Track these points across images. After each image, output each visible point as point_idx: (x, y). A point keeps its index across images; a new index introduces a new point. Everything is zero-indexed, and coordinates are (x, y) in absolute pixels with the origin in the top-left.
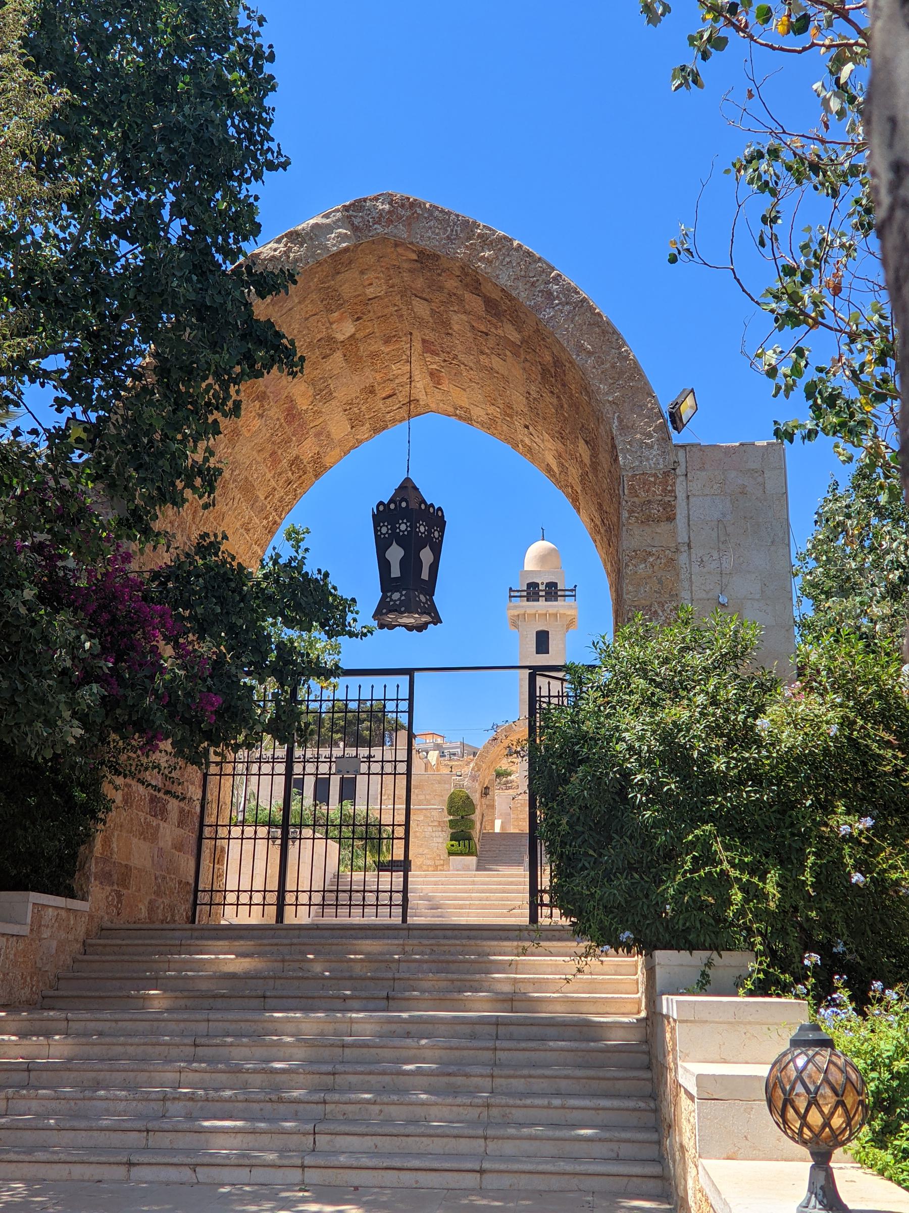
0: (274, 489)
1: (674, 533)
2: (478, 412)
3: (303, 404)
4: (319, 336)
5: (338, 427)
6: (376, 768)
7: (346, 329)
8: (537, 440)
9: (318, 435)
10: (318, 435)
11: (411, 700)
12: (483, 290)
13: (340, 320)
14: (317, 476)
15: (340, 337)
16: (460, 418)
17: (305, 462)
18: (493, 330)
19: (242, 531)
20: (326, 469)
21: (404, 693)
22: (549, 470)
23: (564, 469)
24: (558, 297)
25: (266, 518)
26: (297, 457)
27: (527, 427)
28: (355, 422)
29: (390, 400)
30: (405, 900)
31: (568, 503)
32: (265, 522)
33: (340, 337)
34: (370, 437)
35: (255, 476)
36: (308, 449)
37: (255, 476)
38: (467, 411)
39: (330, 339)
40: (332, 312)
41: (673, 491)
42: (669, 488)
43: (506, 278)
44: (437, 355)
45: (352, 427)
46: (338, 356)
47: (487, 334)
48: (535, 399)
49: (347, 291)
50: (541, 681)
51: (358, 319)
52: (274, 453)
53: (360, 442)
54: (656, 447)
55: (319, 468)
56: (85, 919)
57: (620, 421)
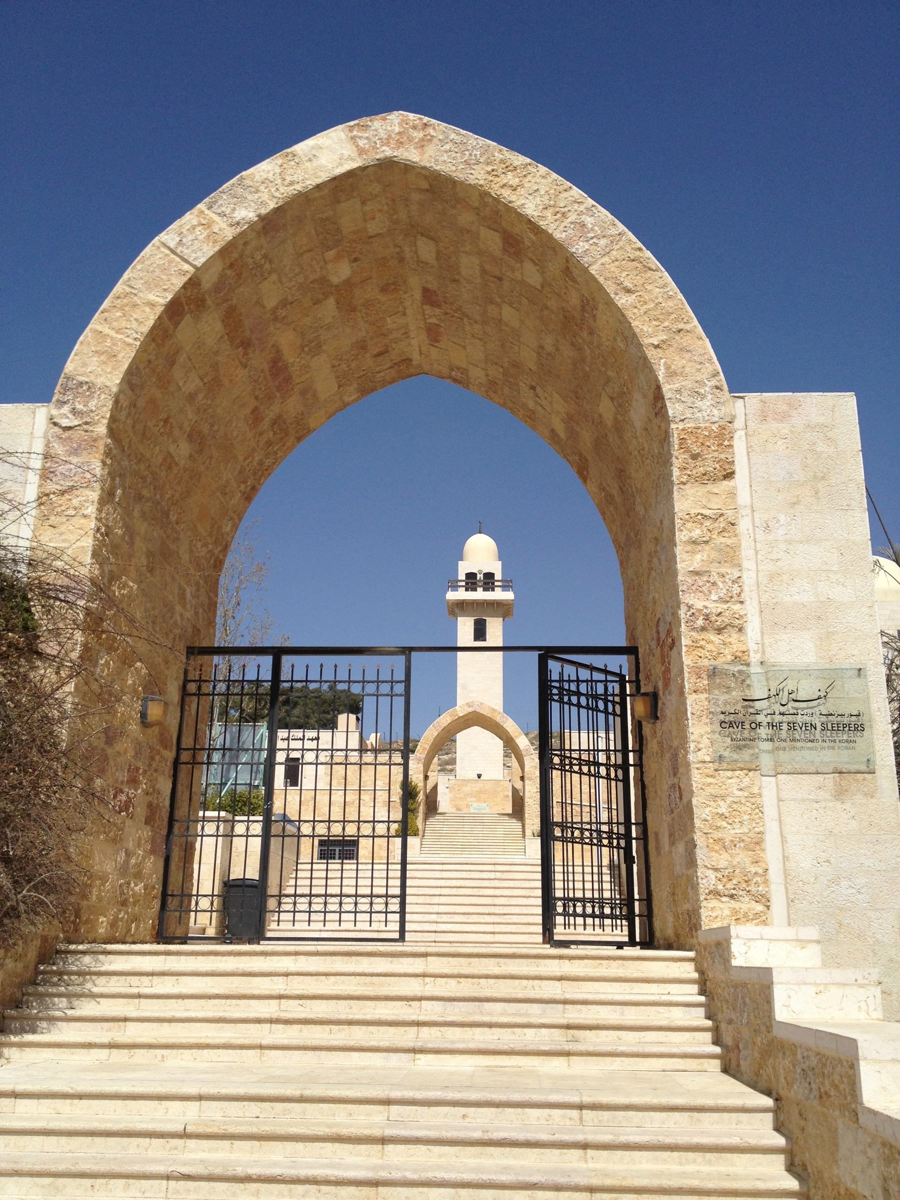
0: (254, 450)
1: (732, 494)
2: (477, 374)
3: (290, 357)
4: (312, 277)
5: (325, 384)
6: (324, 757)
7: (342, 272)
8: (544, 402)
9: (304, 392)
10: (304, 392)
11: (407, 681)
12: (504, 224)
13: (338, 257)
14: (299, 439)
15: (335, 280)
16: (455, 380)
17: (288, 421)
18: (509, 274)
19: (218, 494)
20: (309, 431)
21: (400, 675)
22: (553, 435)
23: (573, 434)
24: (592, 229)
25: (245, 482)
26: (280, 416)
27: (533, 388)
28: (342, 381)
29: (381, 358)
30: (403, 904)
31: (571, 474)
32: (243, 486)
33: (335, 280)
34: (358, 399)
35: (235, 434)
36: (292, 406)
37: (235, 434)
38: (465, 371)
39: (323, 281)
40: (329, 248)
41: (731, 446)
42: (726, 443)
43: (533, 207)
44: (439, 306)
45: (339, 387)
46: (331, 301)
47: (500, 279)
48: (549, 354)
49: (347, 224)
50: (554, 667)
51: (356, 260)
52: (255, 409)
53: (346, 405)
54: (710, 396)
55: (302, 432)
56: (38, 943)
57: (668, 367)
